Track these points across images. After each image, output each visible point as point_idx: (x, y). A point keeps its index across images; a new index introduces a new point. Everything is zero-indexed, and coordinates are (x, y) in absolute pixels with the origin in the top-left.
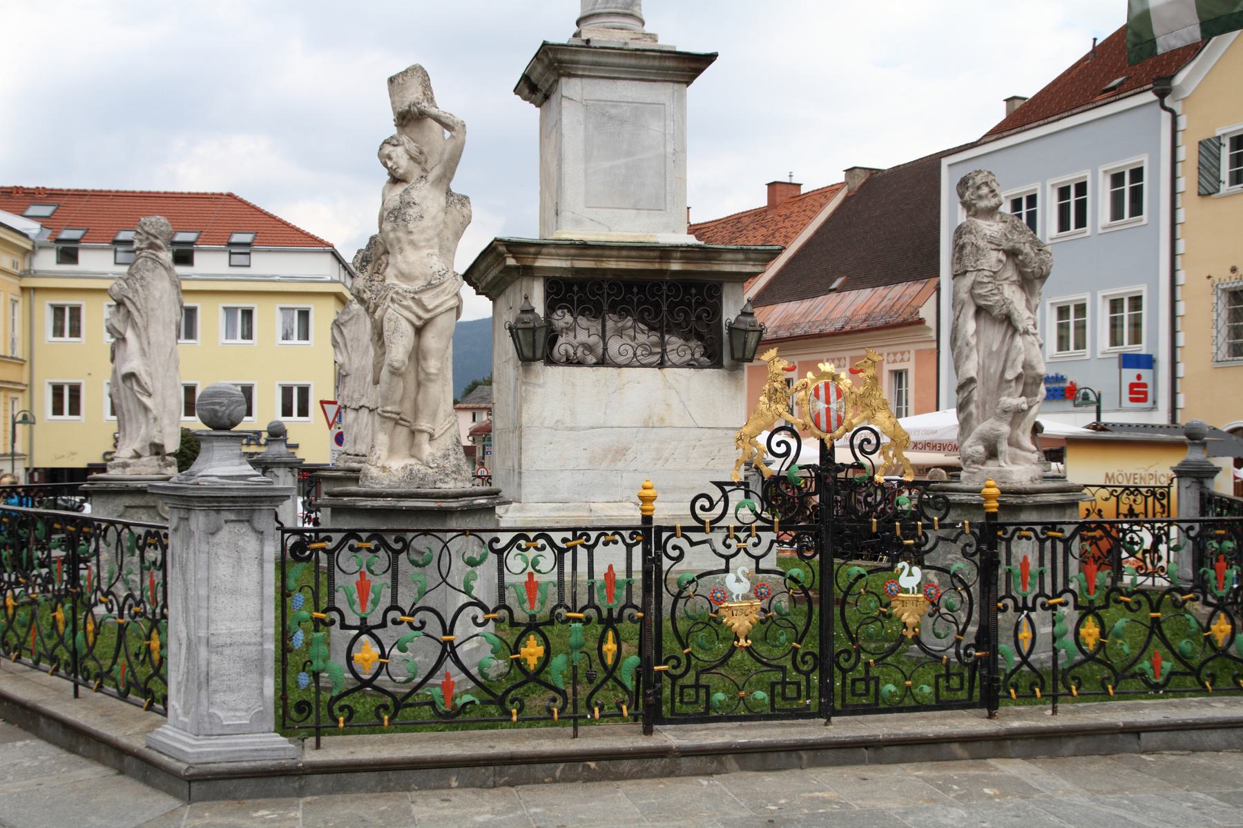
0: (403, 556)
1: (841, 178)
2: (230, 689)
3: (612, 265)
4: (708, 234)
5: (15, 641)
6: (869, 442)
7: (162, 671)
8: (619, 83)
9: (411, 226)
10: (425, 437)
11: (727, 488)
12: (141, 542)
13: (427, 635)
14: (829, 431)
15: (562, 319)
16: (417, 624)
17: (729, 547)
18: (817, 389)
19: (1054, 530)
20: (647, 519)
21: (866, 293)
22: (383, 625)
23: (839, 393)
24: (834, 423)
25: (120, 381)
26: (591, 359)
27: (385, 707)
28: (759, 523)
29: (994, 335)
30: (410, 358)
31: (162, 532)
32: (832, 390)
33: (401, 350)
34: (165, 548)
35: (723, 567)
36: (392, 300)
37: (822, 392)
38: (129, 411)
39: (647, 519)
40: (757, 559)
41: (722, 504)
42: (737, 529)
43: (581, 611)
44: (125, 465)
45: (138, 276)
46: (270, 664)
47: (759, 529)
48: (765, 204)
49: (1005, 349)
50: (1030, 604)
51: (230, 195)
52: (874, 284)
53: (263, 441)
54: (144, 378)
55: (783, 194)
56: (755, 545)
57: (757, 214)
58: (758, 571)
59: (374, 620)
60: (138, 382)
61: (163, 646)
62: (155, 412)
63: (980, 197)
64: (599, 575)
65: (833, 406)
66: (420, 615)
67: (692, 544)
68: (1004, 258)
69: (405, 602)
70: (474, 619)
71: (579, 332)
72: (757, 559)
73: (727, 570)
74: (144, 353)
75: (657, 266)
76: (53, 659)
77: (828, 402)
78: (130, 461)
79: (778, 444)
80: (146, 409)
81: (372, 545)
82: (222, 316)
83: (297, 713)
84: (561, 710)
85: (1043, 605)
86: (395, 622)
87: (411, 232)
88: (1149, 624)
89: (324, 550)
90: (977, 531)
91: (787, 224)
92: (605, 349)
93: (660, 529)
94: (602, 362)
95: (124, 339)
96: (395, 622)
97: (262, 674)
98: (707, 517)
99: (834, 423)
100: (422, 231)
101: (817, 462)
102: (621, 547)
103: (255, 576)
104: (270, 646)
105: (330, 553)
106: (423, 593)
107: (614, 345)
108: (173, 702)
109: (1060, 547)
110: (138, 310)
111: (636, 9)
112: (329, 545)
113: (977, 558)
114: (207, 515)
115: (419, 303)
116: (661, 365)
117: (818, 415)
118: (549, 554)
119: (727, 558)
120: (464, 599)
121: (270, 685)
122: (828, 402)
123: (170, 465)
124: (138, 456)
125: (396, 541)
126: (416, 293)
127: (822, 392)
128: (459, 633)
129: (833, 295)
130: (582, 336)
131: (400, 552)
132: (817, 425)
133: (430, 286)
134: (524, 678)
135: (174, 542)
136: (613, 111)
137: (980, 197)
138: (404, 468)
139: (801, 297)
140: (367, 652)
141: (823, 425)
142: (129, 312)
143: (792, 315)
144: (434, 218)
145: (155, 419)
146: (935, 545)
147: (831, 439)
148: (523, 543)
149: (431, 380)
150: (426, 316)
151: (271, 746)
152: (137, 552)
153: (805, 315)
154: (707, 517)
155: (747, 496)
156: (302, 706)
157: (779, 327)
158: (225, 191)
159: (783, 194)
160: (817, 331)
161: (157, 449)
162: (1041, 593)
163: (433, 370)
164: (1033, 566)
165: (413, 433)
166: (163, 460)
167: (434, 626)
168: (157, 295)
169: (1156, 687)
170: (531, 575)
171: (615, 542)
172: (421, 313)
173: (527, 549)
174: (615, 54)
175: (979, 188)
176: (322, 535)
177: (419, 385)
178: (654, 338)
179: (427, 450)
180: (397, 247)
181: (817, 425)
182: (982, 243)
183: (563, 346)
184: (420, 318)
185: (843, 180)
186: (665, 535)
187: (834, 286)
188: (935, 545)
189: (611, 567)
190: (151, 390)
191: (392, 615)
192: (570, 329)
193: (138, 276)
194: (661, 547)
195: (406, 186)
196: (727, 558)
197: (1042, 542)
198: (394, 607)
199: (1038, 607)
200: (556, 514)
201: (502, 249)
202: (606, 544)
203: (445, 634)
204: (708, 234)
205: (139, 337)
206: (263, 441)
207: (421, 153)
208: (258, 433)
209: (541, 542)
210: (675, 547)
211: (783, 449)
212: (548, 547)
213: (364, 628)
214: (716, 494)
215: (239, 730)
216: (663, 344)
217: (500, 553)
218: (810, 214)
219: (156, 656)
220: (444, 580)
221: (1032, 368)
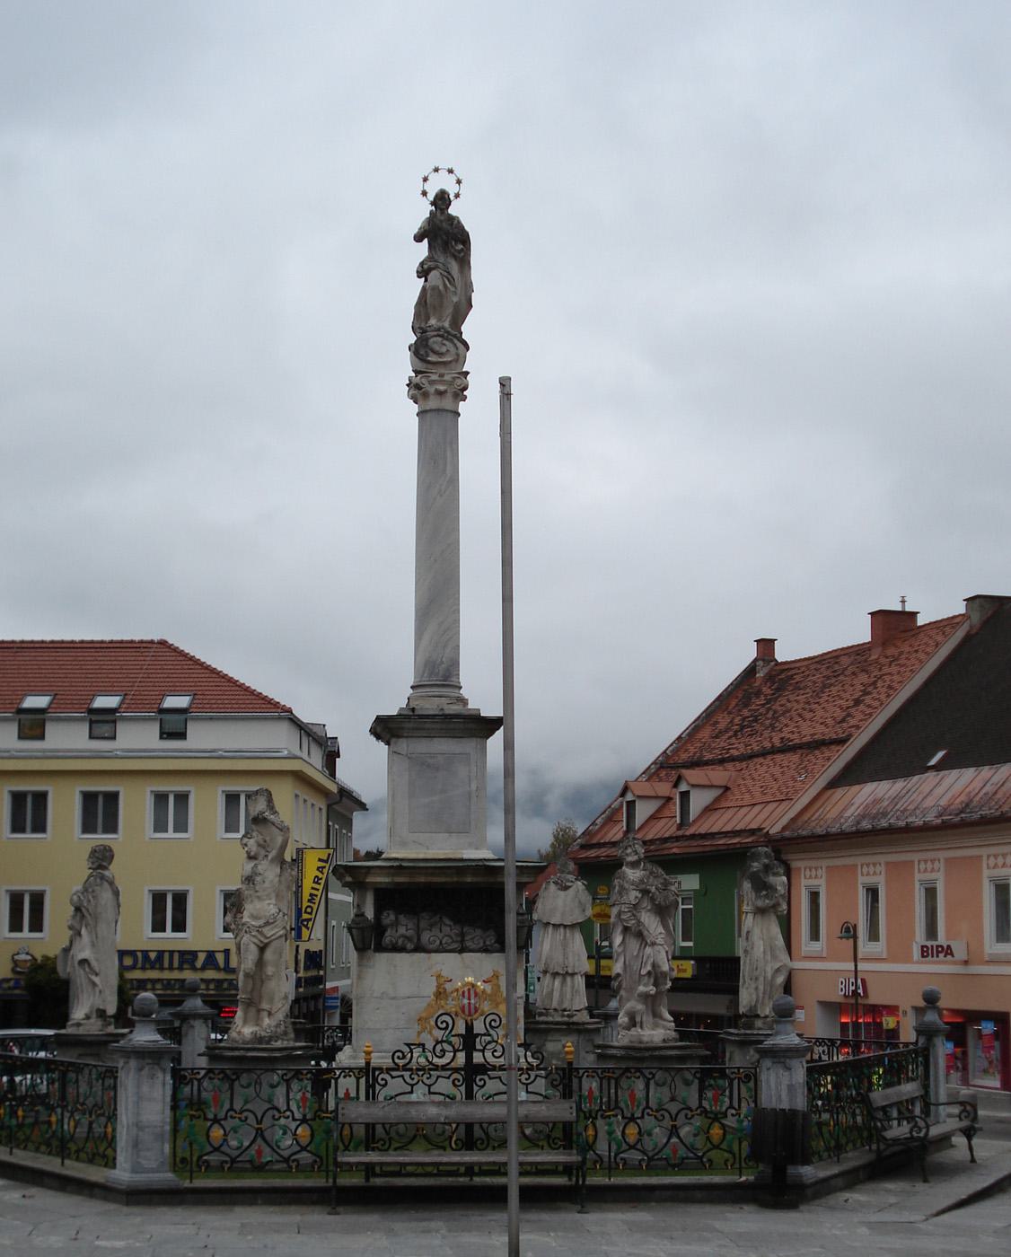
0: (237, 1083)
1: (961, 609)
2: (148, 1150)
3: (422, 879)
4: (798, 678)
5: (23, 1137)
6: (495, 1021)
7: (113, 1145)
8: (435, 740)
9: (257, 888)
10: (265, 1014)
11: (412, 1047)
12: (102, 1076)
13: (248, 1125)
14: (470, 1015)
15: (389, 917)
16: (243, 1119)
17: (413, 1079)
18: (463, 992)
19: (609, 1072)
20: (368, 1064)
21: (970, 773)
22: (225, 1119)
23: (476, 995)
24: (473, 1010)
25: (76, 965)
26: (410, 946)
27: (226, 1162)
28: (431, 1066)
29: (634, 945)
30: (256, 966)
31: (115, 1069)
32: (472, 992)
33: (250, 962)
34: (116, 1078)
35: (410, 1090)
36: (246, 932)
37: (466, 994)
38: (82, 985)
39: (368, 1064)
40: (429, 1086)
41: (410, 1054)
42: (418, 1070)
43: (331, 1113)
44: (78, 1025)
45: (90, 890)
46: (168, 1136)
47: (430, 1069)
48: (868, 639)
49: (641, 954)
50: (594, 1115)
51: (163, 643)
52: (977, 763)
53: (199, 964)
54: (94, 964)
55: (893, 626)
56: (428, 1078)
57: (858, 651)
58: (430, 1093)
59: (221, 1115)
60: (89, 964)
61: (114, 1130)
62: (100, 987)
63: (627, 855)
64: (341, 1095)
65: (472, 1001)
66: (245, 1114)
67: (393, 1077)
68: (640, 896)
69: (237, 1106)
71: (403, 929)
72: (429, 1086)
73: (412, 1092)
74: (93, 945)
75: (455, 879)
76: (48, 1145)
77: (469, 999)
78: (82, 1022)
79: (442, 1023)
80: (94, 984)
81: (221, 1076)
82: (149, 802)
83: (179, 1163)
84: (319, 1168)
85: (602, 1116)
86: (232, 1117)
87: (257, 891)
88: (670, 1128)
89: (196, 1079)
90: (561, 1073)
91: (894, 669)
92: (419, 939)
93: (374, 1069)
94: (419, 948)
95: (79, 934)
96: (232, 1117)
97: (163, 1143)
98: (401, 1062)
99: (473, 1010)
100: (264, 890)
101: (464, 1033)
102: (353, 1079)
103: (161, 1092)
104: (168, 1128)
105: (199, 1080)
106: (246, 1102)
107: (426, 937)
108: (120, 1159)
109: (613, 1082)
110: (90, 914)
111: (454, 679)
112: (615, 1076)
113: (561, 1087)
114: (269, 978)
115: (261, 933)
116: (462, 950)
117: (464, 1007)
119: (412, 1086)
120: (267, 1106)
121: (167, 1148)
122: (469, 999)
123: (110, 1024)
124: (88, 1017)
126: (260, 927)
127: (466, 994)
129: (931, 775)
130: (402, 930)
131: (236, 1080)
132: (463, 1011)
133: (267, 923)
134: (299, 1148)
135: (121, 1074)
136: (431, 761)
137: (627, 855)
138: (252, 1033)
139: (893, 776)
140: (217, 1132)
141: (467, 1012)
142: (83, 915)
143: (880, 800)
144: (272, 881)
145: (100, 992)
146: (535, 1080)
147: (472, 1020)
149: (270, 980)
150: (266, 941)
151: (167, 1177)
152: (100, 1081)
153: (895, 800)
154: (401, 1062)
155: (424, 1051)
156: (183, 1160)
157: (863, 817)
158: (156, 638)
159: (893, 626)
160: (902, 824)
161: (101, 1014)
162: (601, 1109)
163: (270, 973)
164: (597, 1093)
165: (259, 1011)
166: (105, 1020)
167: (252, 1120)
168: (103, 902)
169: (674, 1166)
170: (304, 1093)
171: (350, 1076)
172: (262, 939)
175: (626, 848)
176: (195, 1071)
177: (262, 982)
178: (457, 930)
179: (267, 1021)
180: (250, 900)
181: (463, 1011)
182: (626, 885)
183: (389, 937)
184: (262, 942)
185: (963, 611)
186: (377, 1073)
187: (933, 762)
188: (535, 1080)
189: (347, 1090)
190: (97, 971)
191: (231, 1113)
192: (396, 924)
193: (90, 890)
194: (375, 1080)
195: (256, 862)
196: (412, 1086)
197: (601, 1079)
198: (232, 1109)
199: (599, 1117)
200: (380, 1061)
201: (342, 870)
202: (345, 1077)
203: (258, 1124)
204: (798, 678)
205: (90, 933)
206: (199, 964)
207: (265, 841)
208: (194, 954)
210: (382, 1079)
211: (444, 1025)
214: (406, 1049)
215: (153, 1171)
216: (462, 935)
217: (287, 1081)
218: (921, 656)
219: (110, 1136)
220: (258, 1096)
221: (659, 967)
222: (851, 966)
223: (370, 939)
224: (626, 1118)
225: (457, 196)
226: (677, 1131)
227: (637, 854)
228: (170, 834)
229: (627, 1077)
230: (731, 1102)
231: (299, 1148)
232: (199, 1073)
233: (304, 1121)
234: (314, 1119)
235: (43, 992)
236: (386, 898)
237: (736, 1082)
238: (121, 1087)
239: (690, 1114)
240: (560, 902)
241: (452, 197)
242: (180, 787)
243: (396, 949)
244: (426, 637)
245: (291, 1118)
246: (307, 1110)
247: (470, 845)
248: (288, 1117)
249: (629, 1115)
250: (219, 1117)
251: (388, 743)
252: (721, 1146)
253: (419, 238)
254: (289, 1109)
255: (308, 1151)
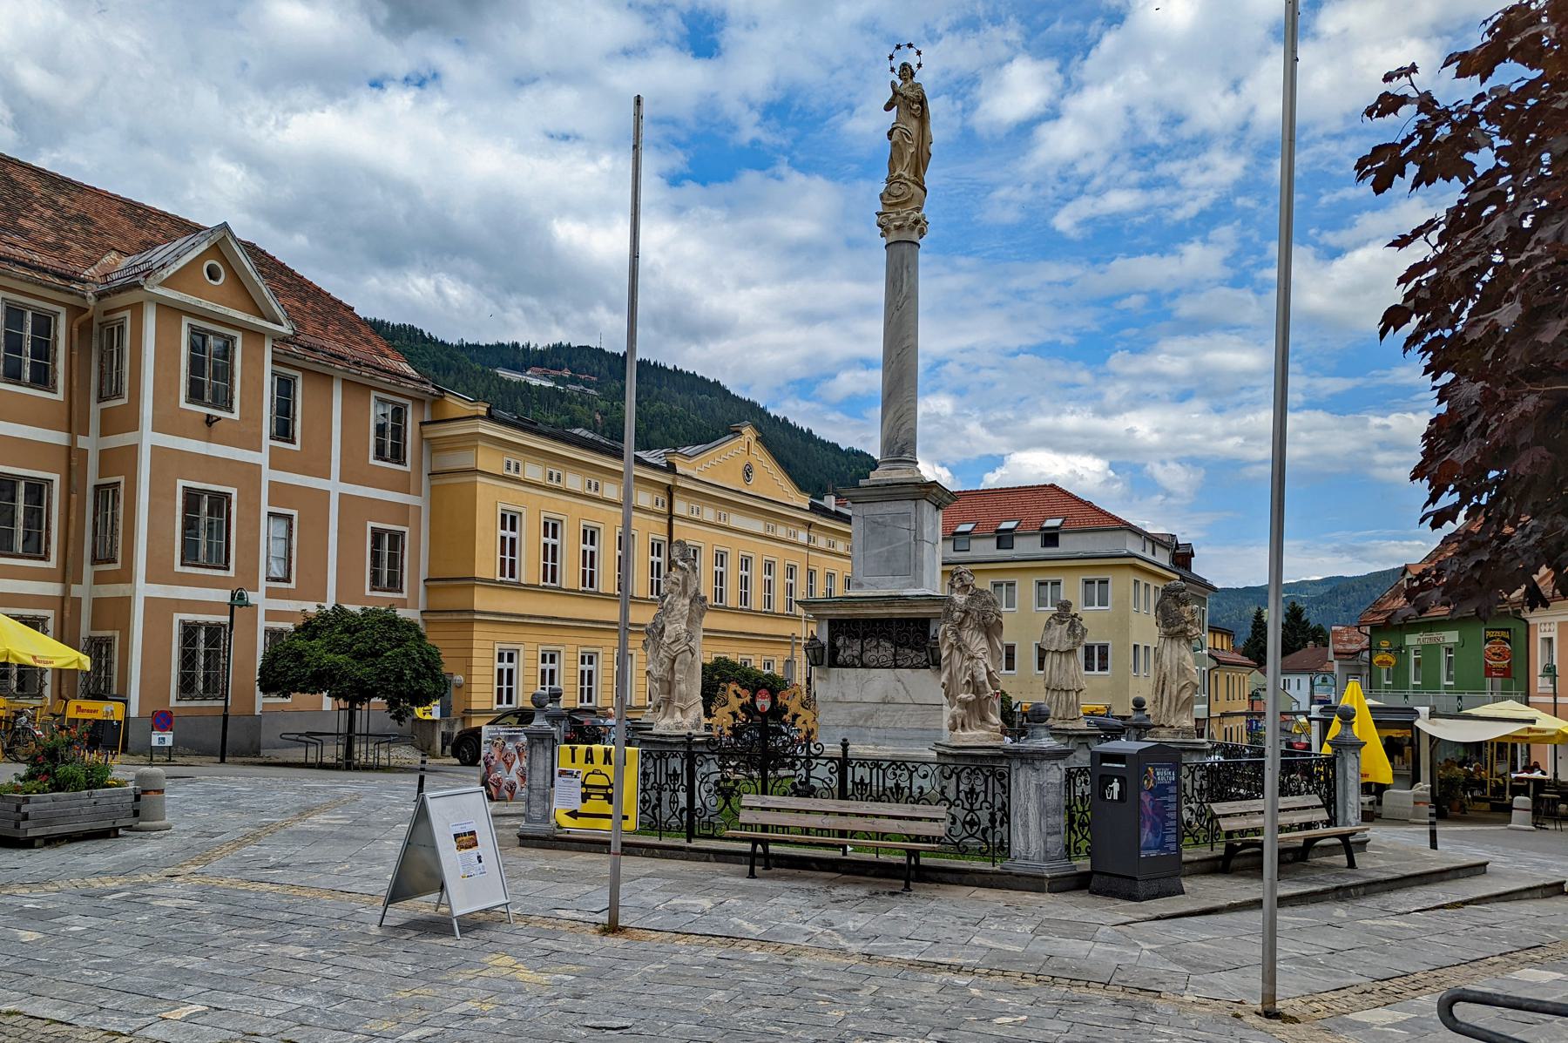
82: (1080, 584)
116: (897, 667)
222: (1559, 700)
223: (824, 657)
225: (919, 65)
228: (1096, 607)
235: (6, 664)
236: (836, 626)
240: (1057, 634)
241: (914, 68)
242: (1103, 577)
243: (845, 665)
244: (890, 415)
247: (911, 586)
253: (888, 107)
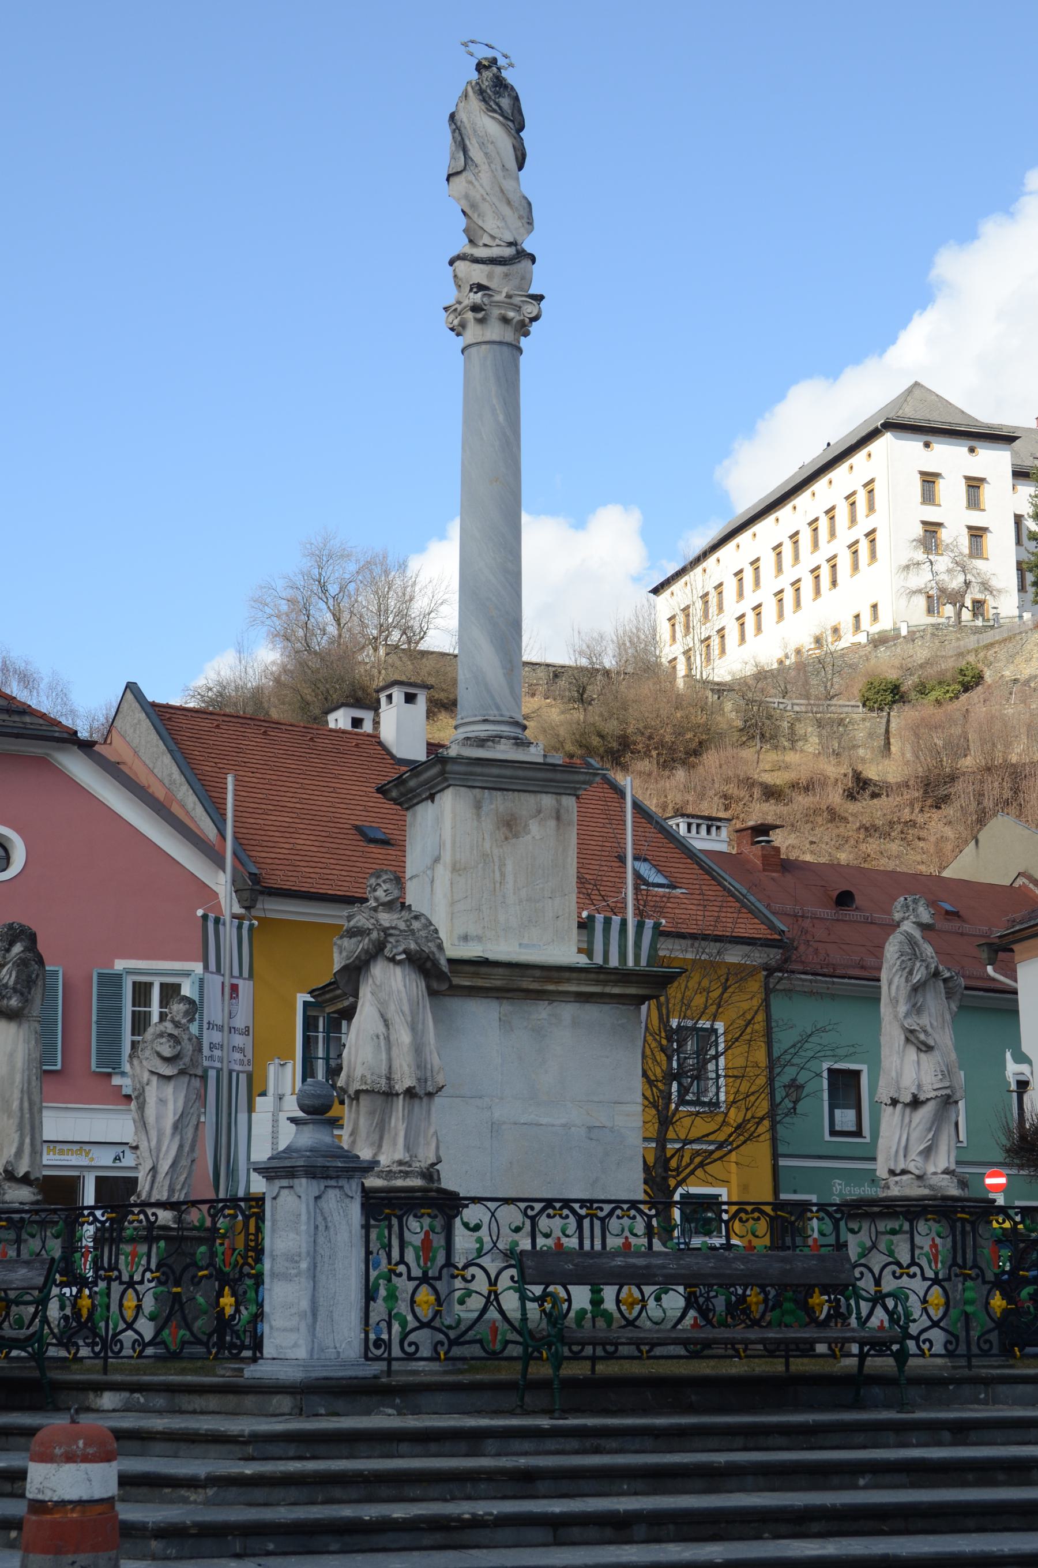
27: (442, 1343)
66: (473, 1270)
70: (894, 1273)
105: (602, 1220)
112: (601, 1214)
118: (572, 1220)
125: (581, 1207)
128: (500, 1287)
148: (743, 1215)
173: (747, 1220)
174: (548, 770)
209: (756, 1215)
212: (571, 1215)
213: (425, 1279)
224: (989, 1282)
226: (497, 1299)
227: (664, 810)
229: (549, 1216)
230: (149, 1262)
231: (929, 1323)
232: (602, 1209)
233: (936, 1281)
234: (948, 1279)
237: (586, 1222)
238: (273, 1231)
239: (898, 1271)
245: (405, 1276)
246: (940, 1265)
248: (914, 1275)
249: (933, 1276)
250: (430, 1274)
251: (403, 566)
252: (941, 1324)
254: (914, 1263)
255: (942, 1328)
